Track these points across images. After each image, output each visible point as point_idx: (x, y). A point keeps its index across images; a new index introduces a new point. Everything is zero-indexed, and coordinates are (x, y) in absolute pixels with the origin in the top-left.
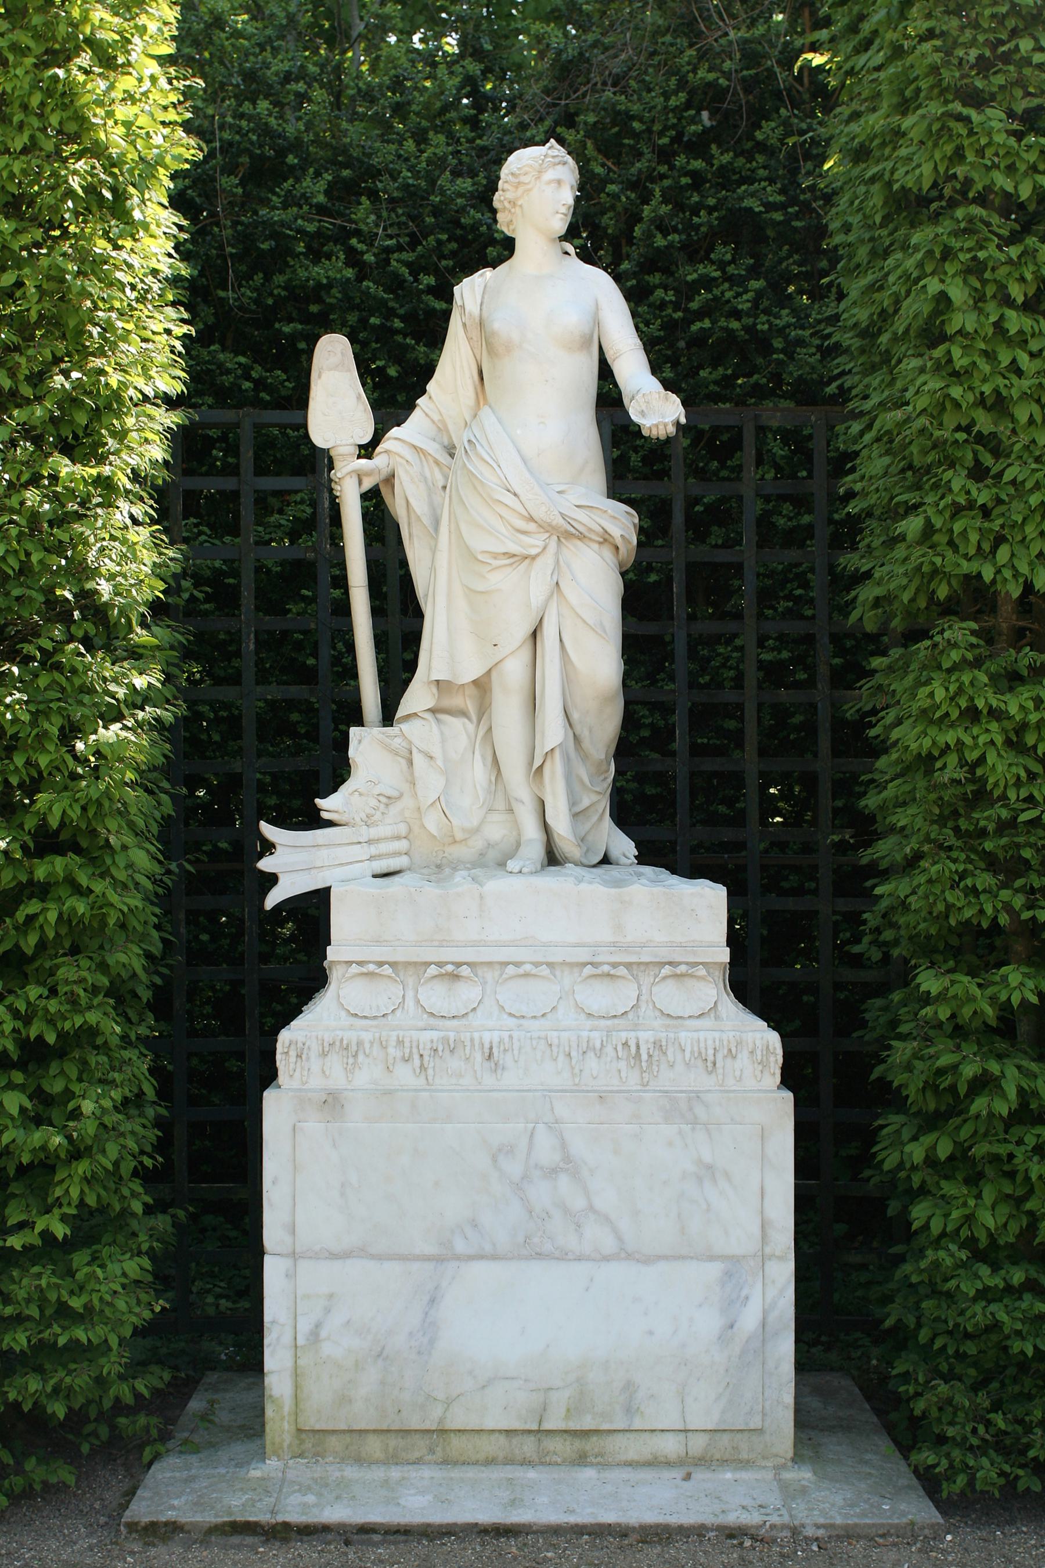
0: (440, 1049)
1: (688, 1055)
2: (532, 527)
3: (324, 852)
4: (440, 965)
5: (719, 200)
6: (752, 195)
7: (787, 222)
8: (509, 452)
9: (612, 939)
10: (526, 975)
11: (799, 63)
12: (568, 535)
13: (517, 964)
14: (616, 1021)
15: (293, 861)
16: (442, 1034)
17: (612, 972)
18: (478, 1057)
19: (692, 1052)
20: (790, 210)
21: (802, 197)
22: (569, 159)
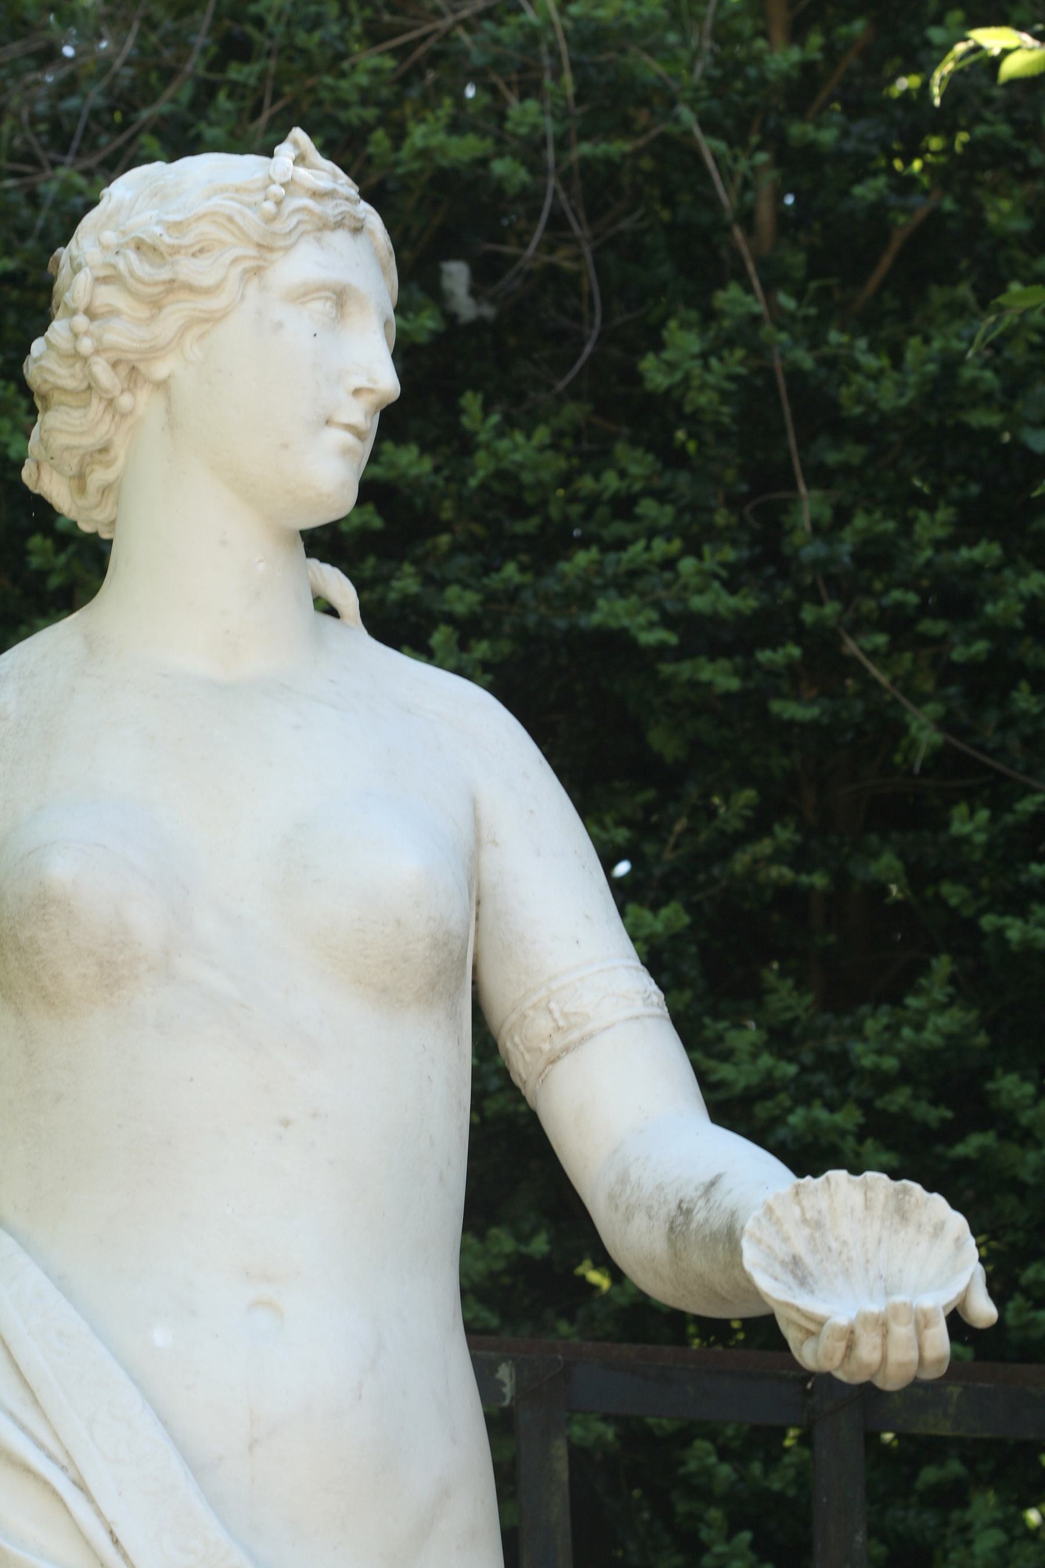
5: (490, 598)
6: (626, 583)
7: (750, 704)
11: (948, 67)
20: (764, 656)
21: (808, 614)
22: (374, 220)
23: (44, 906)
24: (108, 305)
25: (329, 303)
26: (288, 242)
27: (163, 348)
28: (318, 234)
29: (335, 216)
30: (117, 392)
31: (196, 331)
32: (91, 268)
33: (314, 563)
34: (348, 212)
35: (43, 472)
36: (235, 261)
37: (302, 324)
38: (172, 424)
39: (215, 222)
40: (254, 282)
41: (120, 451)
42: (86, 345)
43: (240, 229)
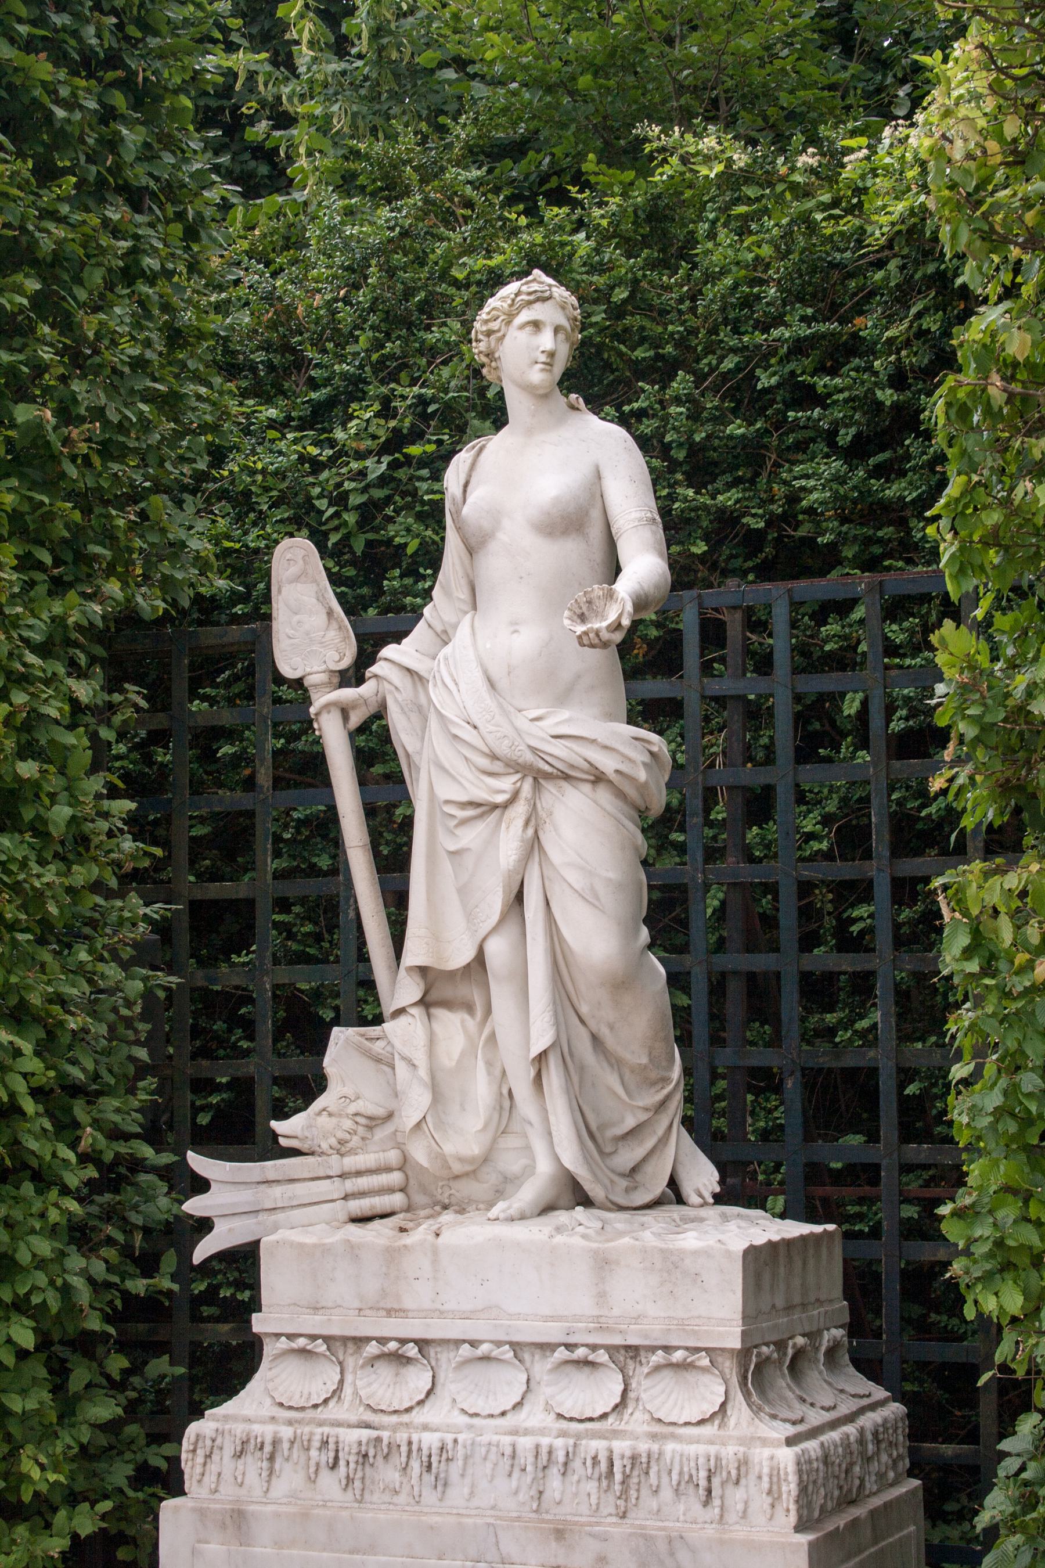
0: (371, 1453)
1: (675, 1476)
2: (498, 767)
3: (277, 1191)
4: (382, 1341)
8: (506, 666)
9: (596, 1313)
10: (486, 1358)
12: (548, 776)
13: (474, 1344)
14: (589, 1425)
15: (231, 1199)
16: (374, 1434)
17: (591, 1358)
18: (415, 1466)
19: (681, 1473)
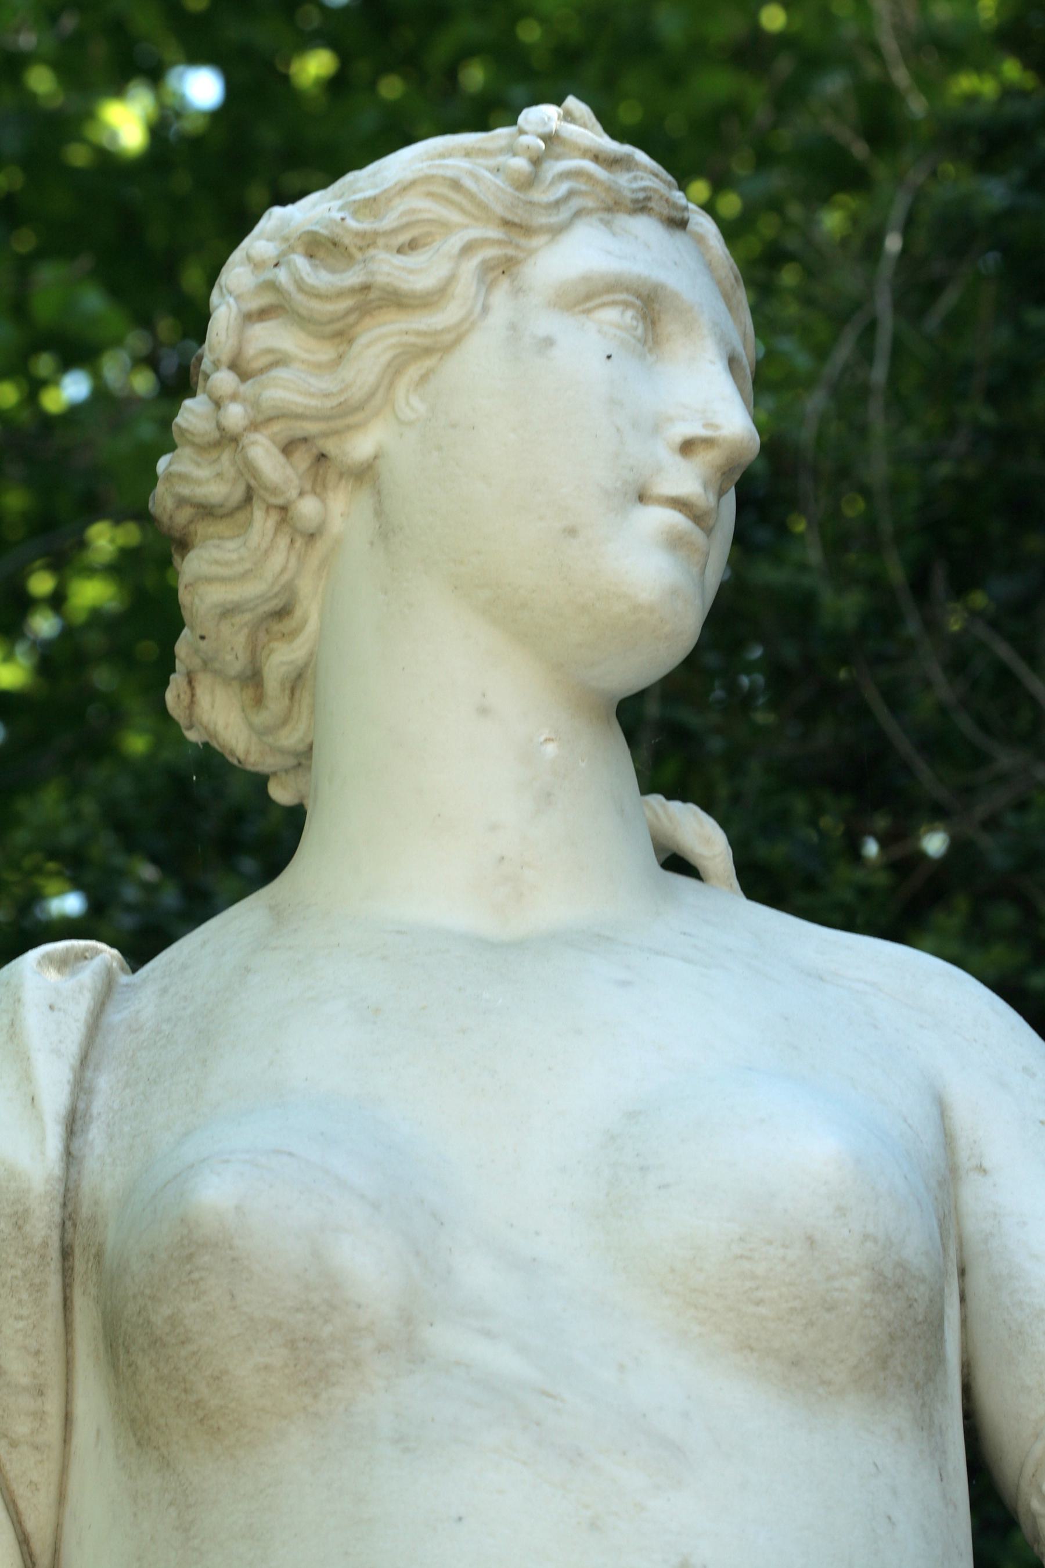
23: (190, 1257)
24: (270, 351)
25: (629, 313)
26: (555, 219)
27: (360, 407)
28: (606, 216)
29: (633, 191)
30: (293, 493)
31: (413, 372)
32: (237, 298)
33: (656, 800)
34: (655, 191)
35: (199, 691)
36: (468, 249)
37: (587, 346)
38: (386, 529)
39: (430, 195)
40: (505, 284)
41: (310, 609)
42: (235, 415)
43: (471, 196)
